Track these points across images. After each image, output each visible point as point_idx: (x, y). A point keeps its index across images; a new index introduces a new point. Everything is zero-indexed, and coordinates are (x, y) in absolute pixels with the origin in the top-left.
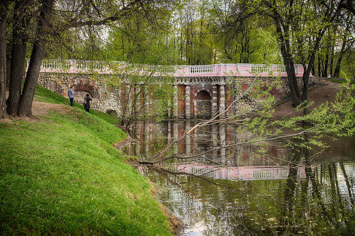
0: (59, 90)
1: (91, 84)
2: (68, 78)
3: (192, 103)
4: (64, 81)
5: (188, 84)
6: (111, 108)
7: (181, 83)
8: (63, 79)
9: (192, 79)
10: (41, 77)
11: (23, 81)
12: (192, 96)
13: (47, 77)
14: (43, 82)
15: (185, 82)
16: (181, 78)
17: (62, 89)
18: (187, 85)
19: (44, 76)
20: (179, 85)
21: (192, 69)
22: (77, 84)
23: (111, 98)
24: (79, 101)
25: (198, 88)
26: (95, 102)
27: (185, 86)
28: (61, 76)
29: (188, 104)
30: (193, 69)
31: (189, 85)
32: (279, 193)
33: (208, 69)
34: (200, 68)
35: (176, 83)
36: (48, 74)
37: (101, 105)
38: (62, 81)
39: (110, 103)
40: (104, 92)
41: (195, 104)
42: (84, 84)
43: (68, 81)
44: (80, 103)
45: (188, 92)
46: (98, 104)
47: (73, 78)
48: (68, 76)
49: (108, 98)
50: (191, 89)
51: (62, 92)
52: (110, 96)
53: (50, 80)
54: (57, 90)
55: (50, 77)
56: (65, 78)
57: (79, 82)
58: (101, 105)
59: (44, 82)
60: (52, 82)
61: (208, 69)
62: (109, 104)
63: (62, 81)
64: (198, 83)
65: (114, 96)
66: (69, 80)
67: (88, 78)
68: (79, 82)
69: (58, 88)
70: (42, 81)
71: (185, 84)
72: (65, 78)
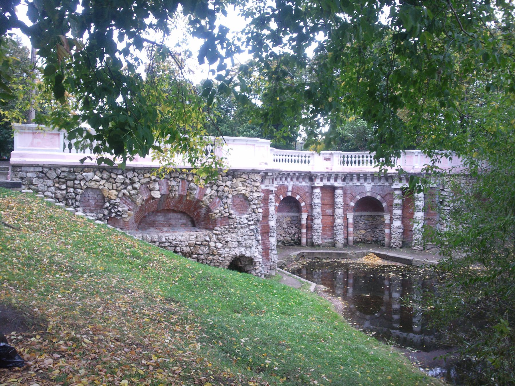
0: (110, 212)
1: (196, 193)
2: (137, 179)
3: (346, 219)
4: (126, 188)
5: (341, 185)
6: (238, 251)
7: (329, 184)
8: (123, 183)
9: (347, 177)
10: (57, 179)
11: (386, 263)
12: (346, 207)
13: (76, 179)
14: (64, 192)
15: (329, 180)
16: (329, 176)
17: (119, 211)
18: (340, 187)
19: (65, 174)
20: (323, 189)
21: (344, 157)
22: (159, 196)
23: (242, 228)
24: (164, 240)
25: (358, 193)
26: (206, 241)
27: (333, 189)
28: (117, 175)
29: (339, 221)
30: (346, 159)
31: (342, 188)
32: (397, 347)
33: (297, 158)
34: (300, 155)
35: (318, 183)
36: (80, 169)
37: (219, 245)
38: (119, 189)
39: (240, 239)
40: (228, 214)
41: (351, 221)
42: (177, 196)
43: (134, 188)
44: (167, 244)
45: (339, 200)
46: (212, 244)
47: (148, 180)
48: (136, 174)
49: (236, 228)
50: (345, 193)
51: (119, 218)
52: (240, 223)
53: (85, 187)
54: (104, 215)
55: (84, 179)
56: (128, 181)
57: (164, 191)
58: (219, 245)
59: (67, 193)
60: (90, 194)
61: (297, 158)
62: (238, 242)
63: (119, 189)
64: (358, 184)
65: (249, 223)
66: (137, 185)
67: (188, 181)
68: (164, 191)
69: (107, 208)
70: (60, 189)
71: (336, 184)
72: (128, 181)
